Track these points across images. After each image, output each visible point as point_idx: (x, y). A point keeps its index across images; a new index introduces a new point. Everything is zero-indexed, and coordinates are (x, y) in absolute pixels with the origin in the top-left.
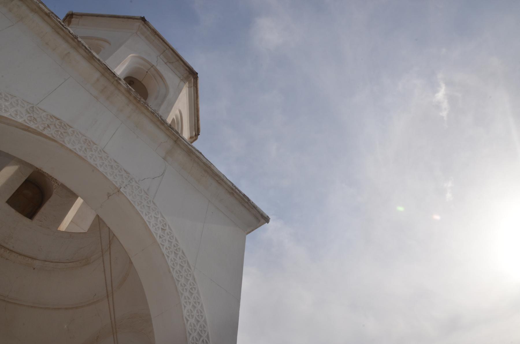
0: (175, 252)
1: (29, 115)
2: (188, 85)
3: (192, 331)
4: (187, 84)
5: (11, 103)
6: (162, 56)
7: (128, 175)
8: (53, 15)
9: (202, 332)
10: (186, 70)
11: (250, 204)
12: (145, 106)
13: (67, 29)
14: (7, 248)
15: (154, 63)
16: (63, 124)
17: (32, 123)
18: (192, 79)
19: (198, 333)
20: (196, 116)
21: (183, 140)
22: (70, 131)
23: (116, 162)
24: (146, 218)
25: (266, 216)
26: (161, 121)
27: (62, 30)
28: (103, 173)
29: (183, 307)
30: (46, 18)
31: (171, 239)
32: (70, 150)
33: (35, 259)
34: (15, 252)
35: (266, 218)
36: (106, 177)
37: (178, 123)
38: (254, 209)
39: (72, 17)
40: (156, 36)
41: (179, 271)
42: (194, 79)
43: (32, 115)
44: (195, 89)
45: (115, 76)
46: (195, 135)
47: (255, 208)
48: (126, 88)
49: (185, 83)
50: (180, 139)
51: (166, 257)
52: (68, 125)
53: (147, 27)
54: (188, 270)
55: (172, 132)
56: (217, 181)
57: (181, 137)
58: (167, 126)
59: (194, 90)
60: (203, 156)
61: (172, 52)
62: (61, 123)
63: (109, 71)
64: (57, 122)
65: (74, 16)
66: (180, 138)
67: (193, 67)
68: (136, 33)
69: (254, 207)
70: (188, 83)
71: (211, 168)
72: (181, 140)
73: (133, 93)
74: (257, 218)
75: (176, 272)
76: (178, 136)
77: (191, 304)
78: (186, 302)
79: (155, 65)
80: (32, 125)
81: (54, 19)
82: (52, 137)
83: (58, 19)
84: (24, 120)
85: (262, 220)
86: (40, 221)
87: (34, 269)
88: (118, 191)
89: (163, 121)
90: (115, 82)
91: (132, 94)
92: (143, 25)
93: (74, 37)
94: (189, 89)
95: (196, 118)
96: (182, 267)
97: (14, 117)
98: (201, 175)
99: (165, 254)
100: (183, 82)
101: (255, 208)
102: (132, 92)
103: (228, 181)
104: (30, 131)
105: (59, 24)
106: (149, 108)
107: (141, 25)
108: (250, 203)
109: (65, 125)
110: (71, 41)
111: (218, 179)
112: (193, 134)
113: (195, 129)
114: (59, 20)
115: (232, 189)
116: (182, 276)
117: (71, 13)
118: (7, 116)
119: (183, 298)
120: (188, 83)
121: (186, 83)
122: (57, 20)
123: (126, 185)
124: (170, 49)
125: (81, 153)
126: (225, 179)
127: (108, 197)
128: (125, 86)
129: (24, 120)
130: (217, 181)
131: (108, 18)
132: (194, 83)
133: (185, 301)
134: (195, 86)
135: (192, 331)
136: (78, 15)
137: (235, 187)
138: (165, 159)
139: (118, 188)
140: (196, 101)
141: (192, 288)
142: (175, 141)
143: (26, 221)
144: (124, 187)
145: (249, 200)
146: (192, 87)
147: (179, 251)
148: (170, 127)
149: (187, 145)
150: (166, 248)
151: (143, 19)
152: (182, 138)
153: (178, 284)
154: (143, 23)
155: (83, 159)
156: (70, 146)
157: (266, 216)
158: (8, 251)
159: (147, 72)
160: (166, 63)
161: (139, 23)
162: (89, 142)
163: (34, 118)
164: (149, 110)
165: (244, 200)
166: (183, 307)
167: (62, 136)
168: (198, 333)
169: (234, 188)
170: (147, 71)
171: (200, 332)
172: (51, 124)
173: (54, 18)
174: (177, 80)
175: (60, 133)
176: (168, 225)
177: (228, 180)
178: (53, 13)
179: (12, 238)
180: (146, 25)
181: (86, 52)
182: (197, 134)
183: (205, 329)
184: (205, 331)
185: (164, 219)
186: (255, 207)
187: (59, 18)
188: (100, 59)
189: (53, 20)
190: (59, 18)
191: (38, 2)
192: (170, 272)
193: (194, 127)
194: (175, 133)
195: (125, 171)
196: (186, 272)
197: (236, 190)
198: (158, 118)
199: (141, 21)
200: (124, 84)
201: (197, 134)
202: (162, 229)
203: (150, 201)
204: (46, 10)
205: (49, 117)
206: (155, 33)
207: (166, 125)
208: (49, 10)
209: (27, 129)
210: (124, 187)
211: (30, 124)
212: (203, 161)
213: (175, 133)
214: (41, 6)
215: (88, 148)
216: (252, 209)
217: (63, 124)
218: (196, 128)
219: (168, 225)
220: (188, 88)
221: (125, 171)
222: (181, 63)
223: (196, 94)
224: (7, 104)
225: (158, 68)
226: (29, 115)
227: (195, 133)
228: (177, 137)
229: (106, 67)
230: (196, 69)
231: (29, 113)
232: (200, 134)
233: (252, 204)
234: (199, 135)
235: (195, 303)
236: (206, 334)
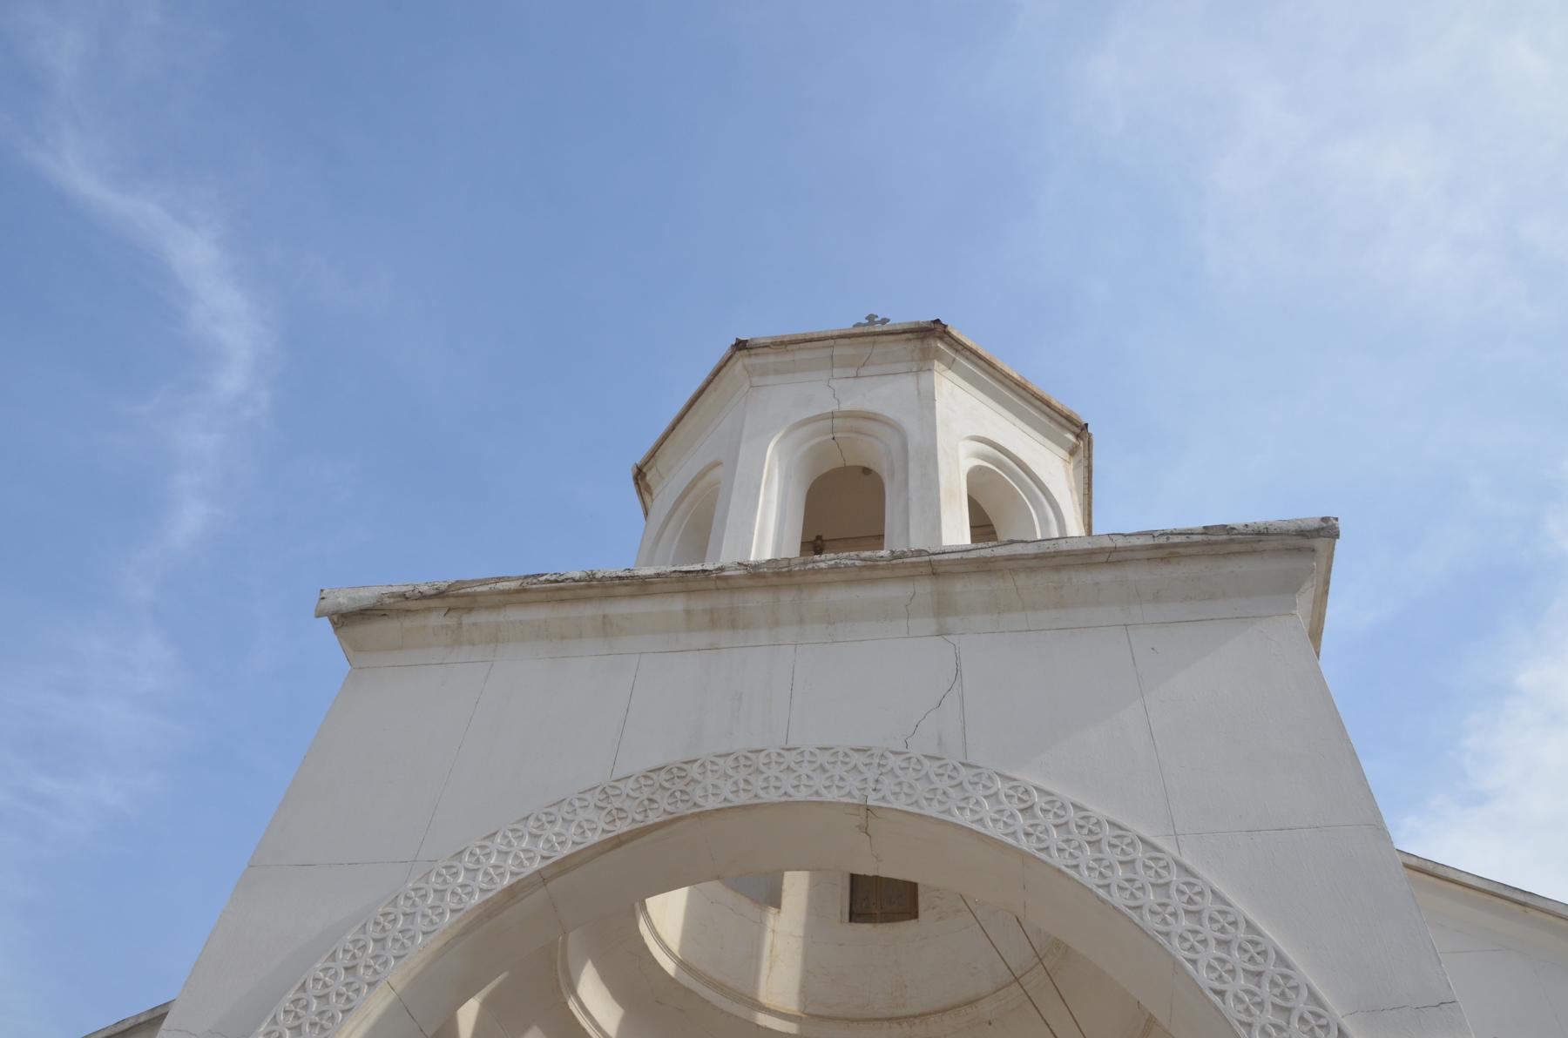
0: (1089, 843)
1: (606, 811)
2: (943, 367)
3: (1251, 1015)
4: (938, 366)
5: (563, 819)
6: (837, 372)
7: (869, 753)
8: (529, 580)
9: (1287, 999)
10: (909, 340)
11: (1240, 536)
12: (809, 569)
13: (567, 579)
14: (911, 1016)
15: (832, 407)
16: (675, 771)
17: (618, 823)
18: (939, 345)
19: (1274, 1005)
20: (1032, 399)
21: (945, 557)
22: (694, 770)
23: (826, 749)
24: (965, 819)
25: (1316, 526)
26: (864, 566)
27: (561, 589)
28: (809, 799)
29: (1189, 966)
30: (525, 597)
31: (1062, 817)
32: (718, 810)
33: (977, 1000)
34: (930, 1014)
35: (1323, 529)
36: (822, 803)
37: (1000, 464)
38: (1263, 537)
39: (645, 475)
40: (790, 347)
41: (1129, 880)
42: (941, 339)
43: (610, 807)
44: (968, 353)
45: (707, 573)
46: (1077, 436)
47: (1263, 534)
48: (746, 572)
49: (930, 370)
50: (934, 561)
51: (1071, 872)
52: (686, 763)
53: (759, 351)
54: (1152, 859)
55: (907, 563)
56: (1107, 562)
57: (936, 554)
58: (885, 563)
59: (967, 358)
60: (1022, 544)
61: (847, 341)
62: (670, 771)
63: (690, 575)
64: (663, 775)
65: (644, 470)
66: (935, 557)
67: (915, 319)
68: (752, 387)
69: (1259, 533)
70: (938, 360)
71: (1062, 552)
72: (940, 561)
73: (765, 570)
74: (1299, 550)
75: (1120, 888)
76: (927, 558)
77: (1213, 943)
78: (1192, 948)
79: (835, 408)
80: (622, 827)
81: (534, 586)
82: (670, 817)
83: (541, 579)
84: (603, 831)
85: (1319, 543)
86: (934, 908)
87: (990, 1024)
88: (868, 810)
89: (869, 563)
90: (720, 584)
91: (765, 573)
92: (750, 355)
93: (586, 581)
94: (953, 371)
95: (1038, 403)
96: (1129, 863)
97: (582, 843)
98: (1055, 588)
99: (1063, 868)
100: (925, 371)
101: (1263, 534)
102: (761, 570)
103: (1129, 538)
104: (627, 841)
105: (548, 585)
106: (818, 564)
107: (747, 361)
108: (1242, 534)
109: (679, 768)
110: (590, 592)
111: (1103, 558)
112: (1070, 441)
113: (1062, 426)
114: (544, 578)
115: (1160, 546)
116: (1142, 888)
117: (636, 470)
118: (569, 853)
119: (1176, 942)
120: (936, 362)
121: (934, 365)
122: (541, 582)
123: (877, 781)
124: (839, 341)
125: (743, 799)
126: (1120, 542)
127: (867, 833)
128: (742, 572)
129: (603, 831)
130: (1107, 562)
131: (690, 412)
132: (950, 346)
133: (1187, 945)
134: (960, 348)
135: (1251, 1015)
136: (648, 462)
137: (1164, 534)
138: (942, 633)
139: (860, 805)
140: (998, 375)
141: (1190, 898)
142: (934, 574)
143: (906, 928)
144: (875, 790)
145: (1227, 529)
146: (954, 360)
147: (1099, 830)
148: (895, 558)
149: (962, 558)
150: (1060, 850)
151: (740, 345)
152: (939, 554)
153: (1142, 918)
154: (745, 352)
155: (755, 806)
156: (712, 804)
157: (1316, 525)
158: (917, 1021)
159: (834, 439)
160: (857, 377)
161: (741, 362)
162: (747, 758)
163: (617, 809)
164: (822, 569)
165: (1215, 543)
166: (1189, 966)
167: (686, 798)
168: (1274, 1005)
169: (1162, 540)
170: (832, 436)
171: (1278, 1001)
172: (653, 793)
173: (535, 584)
174: (906, 384)
175: (678, 794)
176: (1036, 788)
177: (1130, 535)
178: (527, 577)
179: (906, 987)
180: (753, 352)
181: (626, 585)
182: (1077, 430)
183: (1292, 983)
184: (1295, 988)
185: (1015, 780)
186: (1261, 529)
187: (542, 575)
188: (659, 571)
189: (536, 588)
190: (542, 575)
191: (492, 586)
192: (1104, 901)
193: (1053, 425)
194: (914, 559)
195: (857, 750)
196: (1151, 868)
197: (1171, 541)
198: (856, 566)
199: (738, 354)
200: (736, 569)
201: (1082, 431)
202: (1021, 811)
203: (955, 768)
204: (514, 585)
205: (642, 781)
206: (782, 344)
207: (881, 563)
208: (518, 578)
209: (619, 842)
210: (875, 790)
211: (615, 829)
212: (1028, 554)
213: (914, 559)
214: (502, 588)
215: (750, 775)
216: (1260, 541)
217: (675, 771)
218: (1064, 421)
219: (1036, 788)
220: (950, 369)
221: (857, 750)
222: (885, 338)
223: (980, 362)
224: (556, 829)
225: (847, 406)
226: (606, 811)
227: (1074, 433)
228: (926, 562)
229: (681, 574)
230: (925, 317)
231: (603, 808)
232: (1084, 421)
233: (1246, 534)
234: (1086, 425)
235: (1222, 930)
236: (1304, 993)
